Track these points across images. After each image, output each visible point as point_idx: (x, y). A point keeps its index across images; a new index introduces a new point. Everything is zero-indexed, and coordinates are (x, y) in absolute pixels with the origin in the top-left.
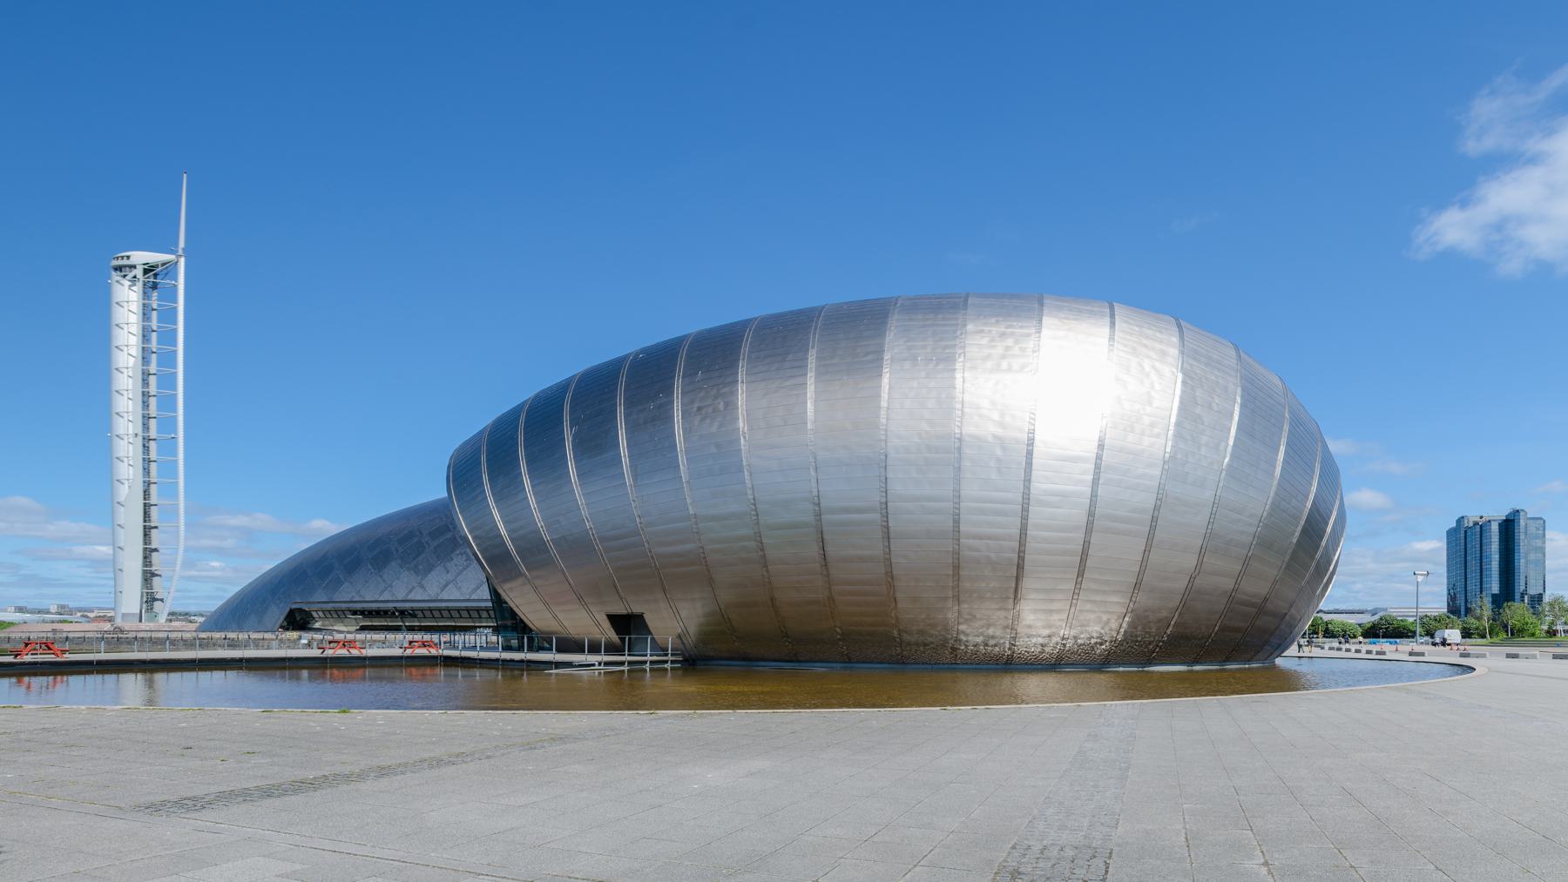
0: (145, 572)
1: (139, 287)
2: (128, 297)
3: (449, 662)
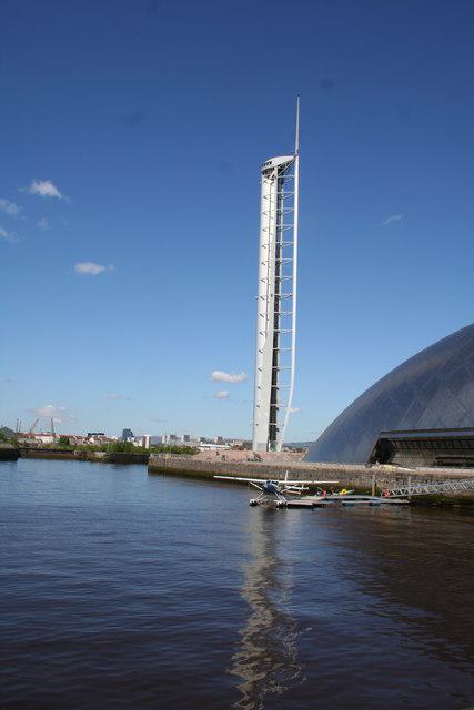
0: (271, 407)
1: (275, 184)
2: (269, 189)
3: (100, 534)
